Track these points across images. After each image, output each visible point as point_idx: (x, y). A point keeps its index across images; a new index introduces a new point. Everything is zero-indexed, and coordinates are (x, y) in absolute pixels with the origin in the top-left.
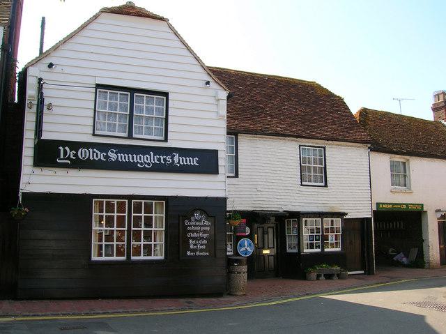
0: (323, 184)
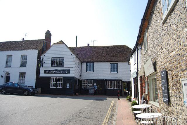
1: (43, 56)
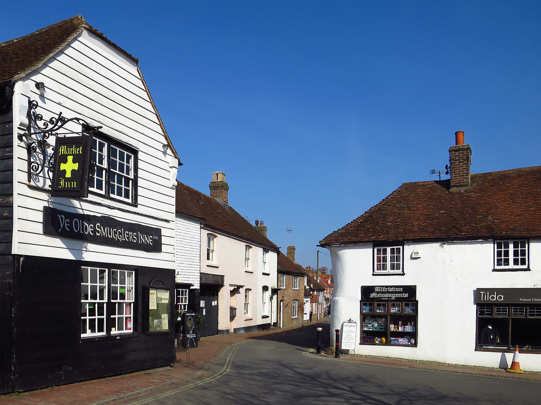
0: (377, 272)
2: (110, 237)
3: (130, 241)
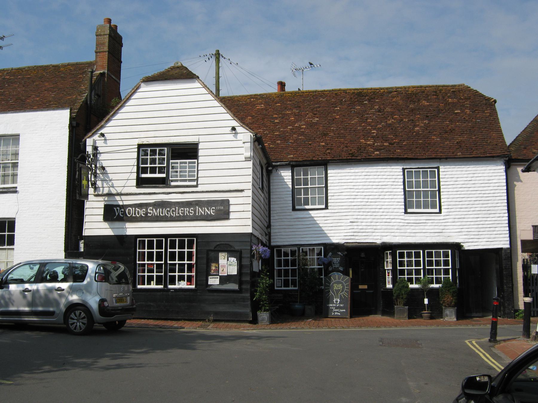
0: (437, 210)
1: (96, 137)
2: (162, 215)
3: (185, 215)
